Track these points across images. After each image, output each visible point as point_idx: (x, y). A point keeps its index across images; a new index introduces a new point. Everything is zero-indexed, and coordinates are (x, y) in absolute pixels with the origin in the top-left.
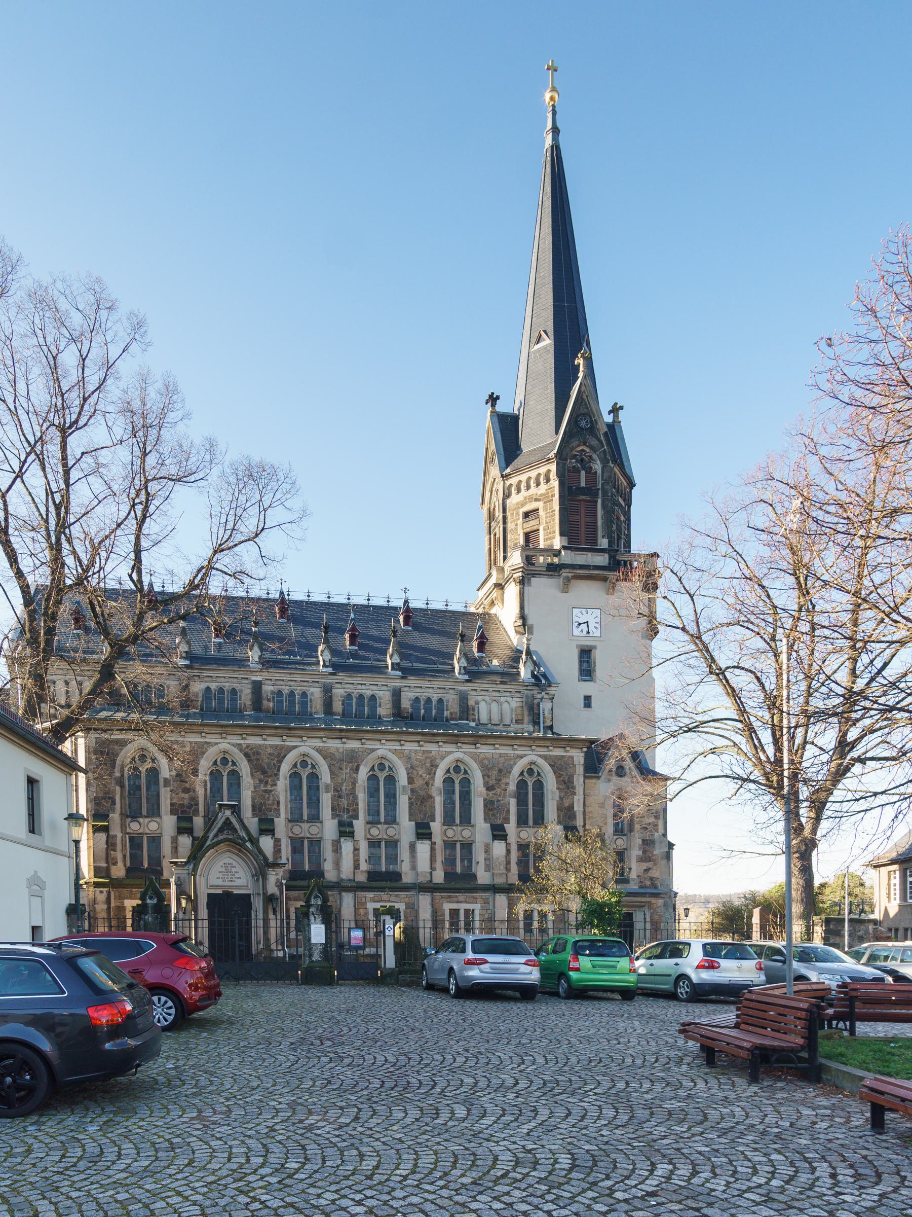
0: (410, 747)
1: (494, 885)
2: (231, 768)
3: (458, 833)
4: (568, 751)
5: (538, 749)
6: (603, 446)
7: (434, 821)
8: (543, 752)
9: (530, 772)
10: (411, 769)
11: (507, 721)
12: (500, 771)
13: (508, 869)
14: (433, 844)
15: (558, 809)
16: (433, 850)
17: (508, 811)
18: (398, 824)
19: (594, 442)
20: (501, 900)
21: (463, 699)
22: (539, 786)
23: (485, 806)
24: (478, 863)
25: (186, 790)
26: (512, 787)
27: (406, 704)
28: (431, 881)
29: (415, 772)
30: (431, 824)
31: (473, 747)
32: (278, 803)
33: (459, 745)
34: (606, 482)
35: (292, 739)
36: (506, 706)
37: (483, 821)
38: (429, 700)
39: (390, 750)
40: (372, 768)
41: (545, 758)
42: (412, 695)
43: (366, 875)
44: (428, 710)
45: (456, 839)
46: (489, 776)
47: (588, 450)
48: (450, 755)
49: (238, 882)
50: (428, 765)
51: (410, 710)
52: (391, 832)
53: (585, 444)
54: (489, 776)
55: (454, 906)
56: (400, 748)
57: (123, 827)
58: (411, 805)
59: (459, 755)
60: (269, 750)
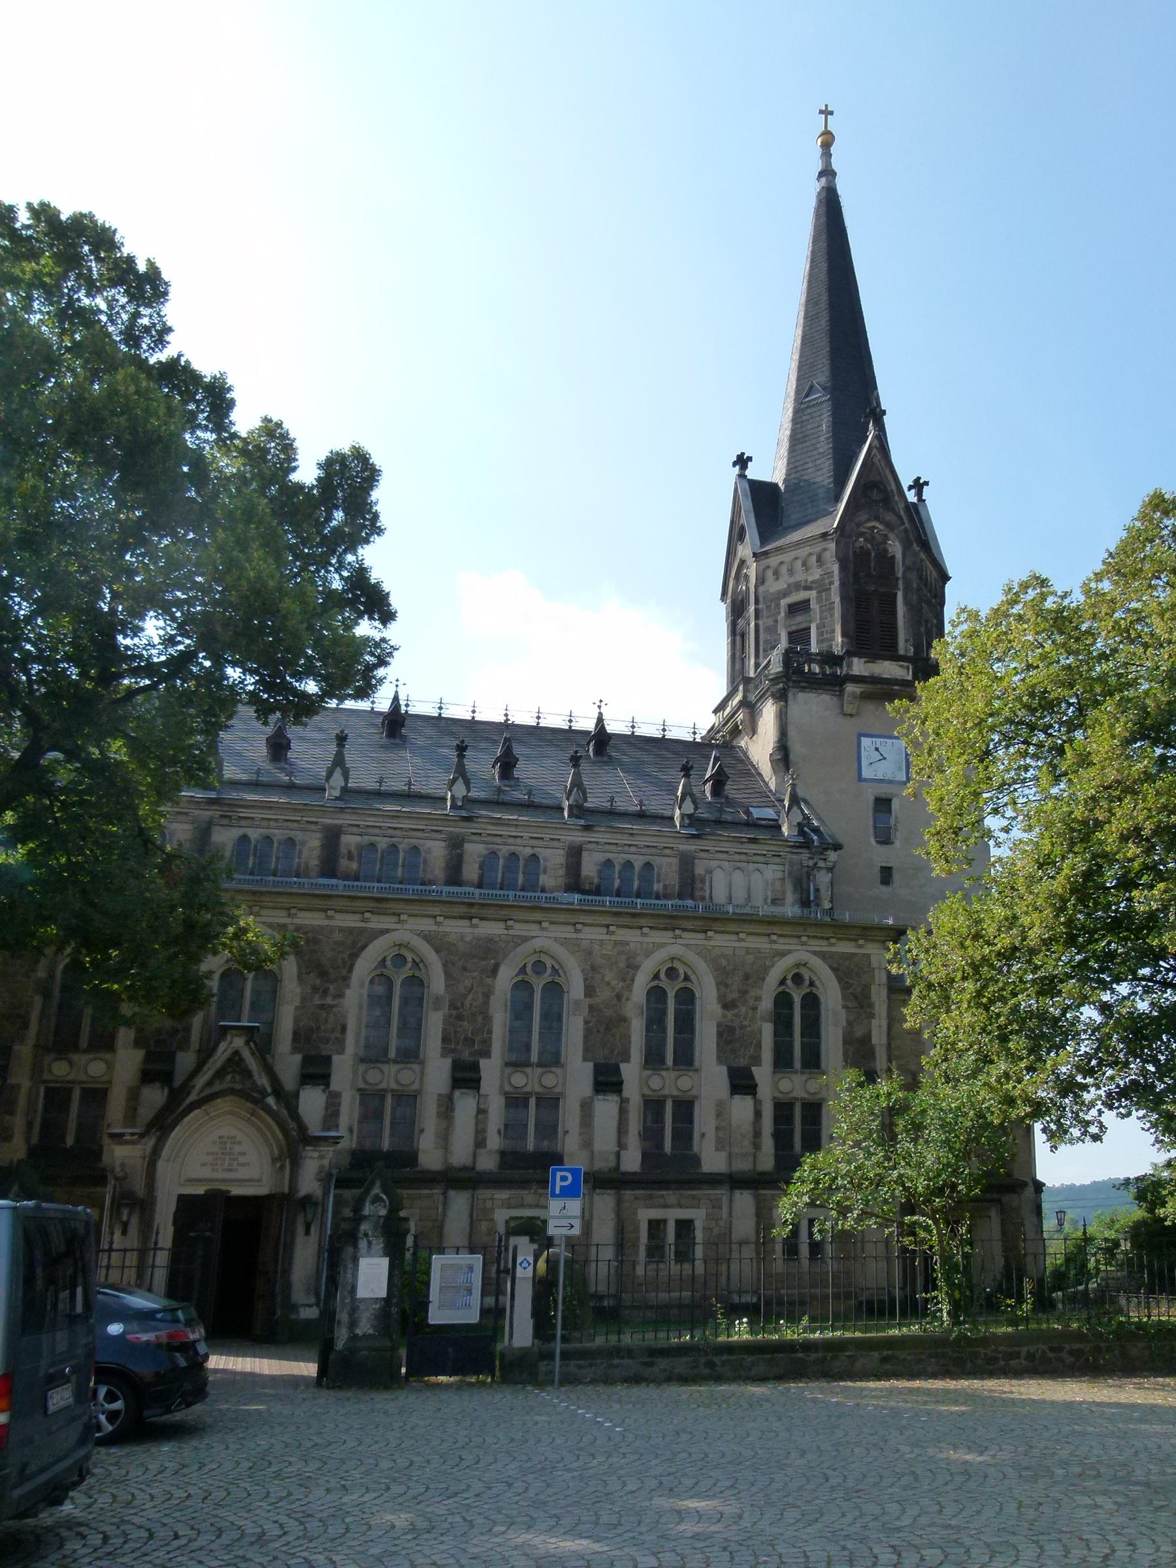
0: (592, 934)
2: (682, 985)
3: (669, 1083)
4: (861, 946)
5: (812, 942)
6: (903, 523)
10: (591, 972)
12: (747, 977)
13: (757, 1146)
14: (624, 1102)
15: (845, 1042)
16: (623, 1111)
17: (759, 1046)
19: (889, 517)
21: (687, 862)
22: (812, 1002)
23: (720, 1034)
24: (703, 1135)
26: (767, 1004)
27: (589, 868)
30: (623, 1066)
31: (702, 936)
32: (344, 1029)
33: (678, 932)
34: (907, 569)
40: (523, 970)
41: (823, 956)
42: (600, 857)
44: (626, 880)
45: (666, 1092)
46: (727, 986)
47: (881, 527)
48: (659, 949)
49: (243, 1173)
50: (622, 965)
51: (596, 881)
52: (549, 1080)
53: (877, 518)
54: (727, 986)
55: (655, 1214)
56: (574, 936)
57: (37, 1069)
58: (588, 1032)
59: (676, 950)
60: (337, 936)
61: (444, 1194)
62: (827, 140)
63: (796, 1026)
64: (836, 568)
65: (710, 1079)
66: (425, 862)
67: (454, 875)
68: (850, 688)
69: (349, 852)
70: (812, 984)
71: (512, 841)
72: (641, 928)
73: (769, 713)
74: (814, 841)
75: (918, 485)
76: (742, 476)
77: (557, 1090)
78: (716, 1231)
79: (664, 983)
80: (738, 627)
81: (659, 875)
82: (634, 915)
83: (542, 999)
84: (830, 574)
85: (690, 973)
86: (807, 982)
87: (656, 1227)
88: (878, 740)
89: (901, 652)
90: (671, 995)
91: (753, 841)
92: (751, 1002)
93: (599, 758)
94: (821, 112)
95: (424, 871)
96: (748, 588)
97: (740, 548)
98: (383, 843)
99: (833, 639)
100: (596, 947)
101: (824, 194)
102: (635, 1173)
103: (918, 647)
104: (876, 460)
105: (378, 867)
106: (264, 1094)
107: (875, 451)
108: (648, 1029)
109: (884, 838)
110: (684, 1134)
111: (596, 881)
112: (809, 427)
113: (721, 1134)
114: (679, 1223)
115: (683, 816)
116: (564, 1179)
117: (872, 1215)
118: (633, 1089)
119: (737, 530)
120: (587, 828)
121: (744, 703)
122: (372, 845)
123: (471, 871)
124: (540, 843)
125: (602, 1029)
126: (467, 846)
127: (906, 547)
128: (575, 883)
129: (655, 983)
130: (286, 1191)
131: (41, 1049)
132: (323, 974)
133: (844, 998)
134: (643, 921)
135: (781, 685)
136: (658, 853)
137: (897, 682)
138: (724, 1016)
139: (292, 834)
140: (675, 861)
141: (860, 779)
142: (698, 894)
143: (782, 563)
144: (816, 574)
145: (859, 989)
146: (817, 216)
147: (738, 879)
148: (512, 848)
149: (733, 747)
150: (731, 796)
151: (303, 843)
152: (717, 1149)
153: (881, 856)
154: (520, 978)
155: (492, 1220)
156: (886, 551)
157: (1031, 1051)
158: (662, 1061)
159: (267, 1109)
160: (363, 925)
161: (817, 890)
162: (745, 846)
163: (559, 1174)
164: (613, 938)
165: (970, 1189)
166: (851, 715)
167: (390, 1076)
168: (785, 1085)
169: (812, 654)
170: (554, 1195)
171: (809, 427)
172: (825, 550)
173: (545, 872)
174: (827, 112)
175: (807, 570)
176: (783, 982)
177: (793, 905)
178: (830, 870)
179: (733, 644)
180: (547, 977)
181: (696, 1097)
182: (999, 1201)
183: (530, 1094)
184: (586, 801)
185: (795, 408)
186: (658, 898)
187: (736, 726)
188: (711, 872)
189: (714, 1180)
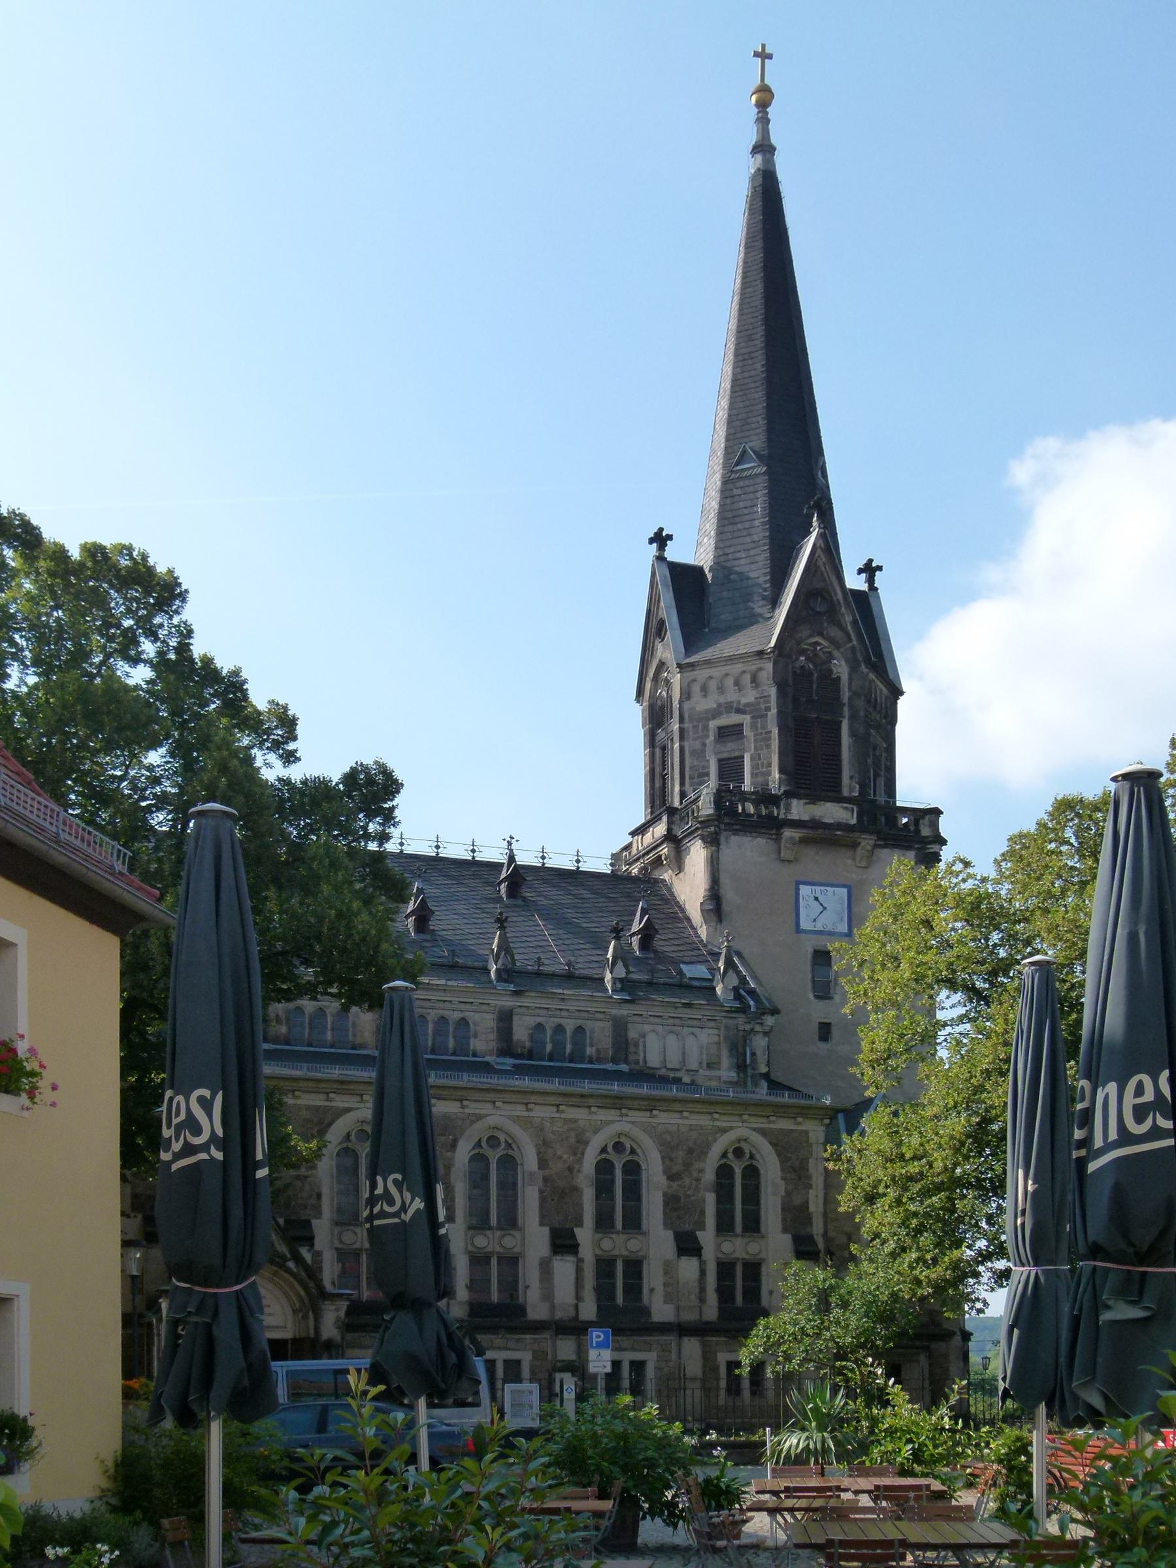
0: (542, 1113)
1: (679, 1325)
2: (630, 1158)
3: (619, 1245)
4: (800, 1123)
5: (753, 1119)
6: (850, 640)
8: (761, 1123)
9: (738, 1152)
10: (543, 1146)
11: (694, 1065)
12: (690, 1151)
13: (702, 1299)
14: (580, 1261)
15: (783, 1209)
16: (579, 1270)
17: (703, 1212)
18: (519, 1229)
19: (834, 632)
20: (692, 1347)
21: (620, 1028)
22: (752, 1173)
23: (666, 1204)
24: (652, 1290)
26: (709, 1176)
27: (521, 1032)
29: (550, 1151)
31: (648, 1114)
32: (319, 1196)
33: (624, 1111)
34: (855, 695)
35: (345, 1098)
36: (690, 1042)
37: (662, 1227)
38: (559, 1029)
39: (509, 1117)
40: (479, 1144)
41: (763, 1132)
42: (531, 1021)
43: (467, 1308)
44: (558, 1044)
45: (616, 1252)
46: (671, 1160)
47: (825, 643)
48: (606, 1128)
50: (573, 1140)
51: (528, 1044)
52: (509, 1242)
53: (821, 634)
54: (671, 1160)
56: (526, 1114)
58: (543, 1201)
60: (305, 1114)
61: (134, 1308)
62: (765, 97)
63: (738, 1191)
64: (773, 692)
65: (658, 1242)
68: (788, 833)
69: (277, 1016)
70: (752, 1157)
71: (440, 1005)
72: (590, 1107)
73: (697, 855)
74: (750, 1003)
75: (869, 570)
76: (660, 558)
77: (517, 1250)
78: (666, 1370)
79: (612, 1156)
80: (658, 739)
81: (591, 1038)
82: (582, 1096)
83: (498, 1169)
84: (766, 698)
85: (635, 1147)
86: (748, 1156)
88: (818, 888)
89: (845, 792)
91: (688, 1006)
92: (695, 1174)
93: (513, 902)
94: (756, 54)
95: (354, 1035)
96: (670, 697)
97: (659, 647)
99: (769, 774)
101: (760, 180)
103: (863, 786)
104: (820, 563)
105: (307, 1031)
106: (284, 1259)
107: (819, 552)
108: (598, 1197)
109: (824, 990)
110: (634, 1287)
111: (528, 1044)
112: (741, 504)
113: (669, 1289)
114: (633, 1363)
115: (614, 980)
116: (598, 1336)
117: (811, 1360)
118: (587, 1252)
119: (654, 623)
120: (517, 993)
121: (669, 837)
124: (468, 1007)
127: (854, 669)
128: (507, 1047)
129: (603, 1156)
130: (312, 1335)
133: (783, 1170)
134: (591, 1101)
135: (712, 829)
136: (588, 1015)
137: (839, 826)
138: (669, 1187)
140: (608, 1025)
141: (798, 930)
142: (631, 1057)
143: (710, 678)
144: (750, 696)
145: (797, 1163)
146: (751, 210)
147: (672, 1041)
148: (441, 1012)
149: (656, 881)
150: (660, 949)
152: (665, 1302)
153: (819, 1011)
154: (476, 1151)
156: (831, 671)
157: (937, 1246)
158: (612, 1226)
159: (288, 1271)
160: (327, 1104)
161: (753, 1054)
162: (680, 1010)
163: (595, 1334)
164: (562, 1116)
165: (885, 1343)
166: (790, 861)
168: (727, 1247)
169: (744, 793)
170: (592, 1347)
171: (741, 504)
172: (760, 669)
173: (475, 1036)
174: (763, 55)
175: (740, 690)
176: (724, 1155)
177: (729, 1069)
178: (766, 1034)
179: (652, 756)
180: (500, 1151)
181: (645, 1257)
182: (928, 1348)
183: (492, 1253)
184: (514, 964)
185: (723, 476)
186: (591, 1062)
187: (660, 856)
188: (644, 1036)
189: (664, 1328)
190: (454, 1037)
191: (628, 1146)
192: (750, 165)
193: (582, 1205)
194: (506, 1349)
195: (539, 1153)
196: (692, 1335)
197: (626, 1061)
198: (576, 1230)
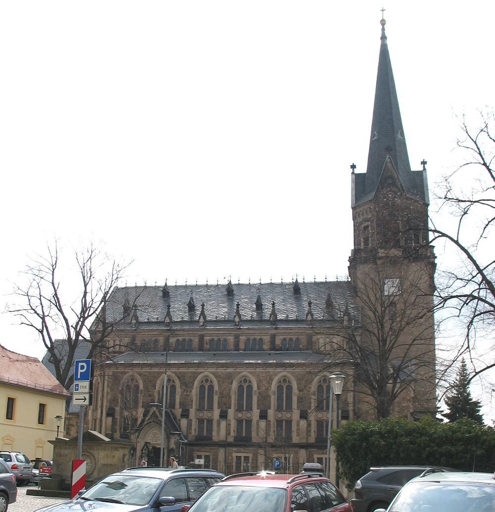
2: (248, 384)
7: (270, 409)
10: (259, 382)
21: (310, 338)
25: (150, 396)
27: (278, 341)
28: (266, 442)
32: (192, 401)
38: (291, 339)
42: (282, 337)
43: (233, 438)
45: (283, 418)
50: (268, 379)
52: (280, 415)
58: (258, 400)
60: (190, 375)
62: (383, 22)
66: (228, 343)
67: (237, 348)
70: (289, 382)
76: (353, 173)
79: (282, 384)
87: (239, 458)
90: (285, 387)
92: (308, 389)
98: (216, 338)
100: (260, 374)
102: (312, 443)
122: (213, 339)
123: (242, 346)
125: (263, 400)
126: (241, 337)
131: (122, 409)
132: (186, 386)
139: (191, 337)
151: (194, 340)
155: (232, 456)
167: (206, 415)
190: (258, 345)
191: (287, 380)
192: (379, 42)
193: (270, 401)
194: (205, 451)
195: (257, 384)
196: (222, 447)
197: (311, 349)
198: (190, 409)
